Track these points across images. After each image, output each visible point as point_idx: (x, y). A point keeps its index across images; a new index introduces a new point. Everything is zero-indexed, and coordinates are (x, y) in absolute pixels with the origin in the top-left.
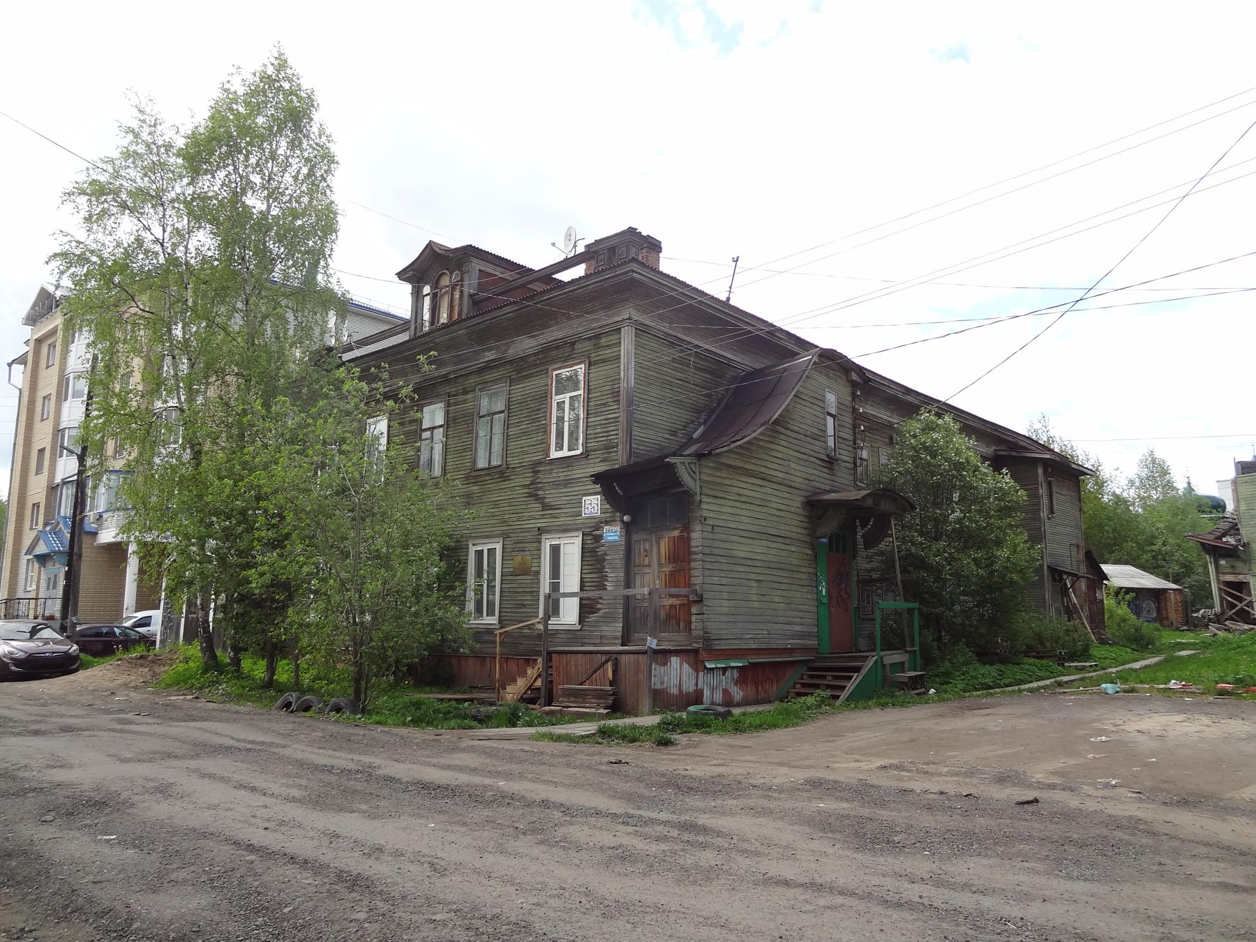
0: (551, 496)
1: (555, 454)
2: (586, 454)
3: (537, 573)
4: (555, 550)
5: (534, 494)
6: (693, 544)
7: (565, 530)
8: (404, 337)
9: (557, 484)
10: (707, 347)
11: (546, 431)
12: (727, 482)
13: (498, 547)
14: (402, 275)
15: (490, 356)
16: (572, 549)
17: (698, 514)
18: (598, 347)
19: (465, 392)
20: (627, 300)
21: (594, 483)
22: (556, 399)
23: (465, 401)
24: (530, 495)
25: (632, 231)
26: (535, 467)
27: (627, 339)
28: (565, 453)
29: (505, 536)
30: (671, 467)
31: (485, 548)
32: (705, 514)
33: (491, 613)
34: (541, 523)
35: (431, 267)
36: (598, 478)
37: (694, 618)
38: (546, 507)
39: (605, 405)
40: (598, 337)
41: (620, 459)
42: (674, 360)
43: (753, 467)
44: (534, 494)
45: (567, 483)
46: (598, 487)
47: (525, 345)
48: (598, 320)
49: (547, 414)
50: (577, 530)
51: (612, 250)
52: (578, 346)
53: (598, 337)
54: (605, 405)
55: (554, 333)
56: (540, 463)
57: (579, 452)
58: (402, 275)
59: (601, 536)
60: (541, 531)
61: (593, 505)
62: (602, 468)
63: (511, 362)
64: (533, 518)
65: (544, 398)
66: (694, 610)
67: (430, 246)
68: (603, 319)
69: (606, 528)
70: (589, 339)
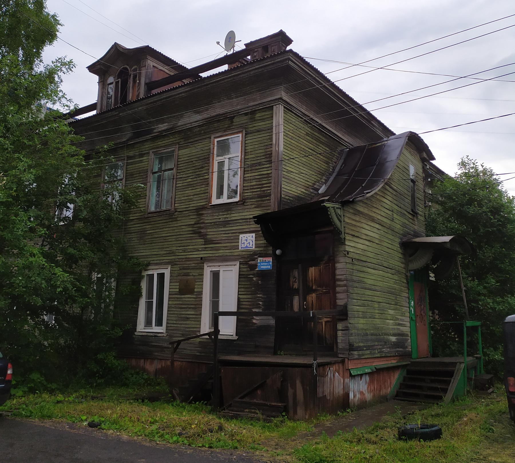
0: (212, 233)
1: (215, 201)
2: (243, 202)
3: (201, 293)
4: (216, 276)
5: (198, 232)
6: (338, 272)
7: (225, 259)
8: (94, 113)
9: (216, 225)
10: (320, 122)
11: (207, 183)
12: (358, 224)
13: (167, 272)
14: (92, 68)
15: (163, 127)
16: (230, 277)
17: (342, 249)
18: (253, 120)
19: (142, 155)
20: (281, 84)
21: (256, 223)
22: (217, 159)
23: (141, 162)
24: (194, 232)
25: (148, 46)
26: (199, 211)
27: (279, 114)
28: (224, 200)
29: (172, 263)
30: (326, 209)
31: (155, 273)
32: (348, 248)
33: (159, 323)
34: (203, 254)
35: (119, 65)
36: (259, 219)
37: (339, 333)
38: (208, 242)
39: (260, 164)
40: (253, 113)
41: (273, 206)
42: (307, 134)
43: (374, 215)
44: (198, 232)
45: (226, 223)
46: (258, 227)
47: (191, 119)
48: (254, 100)
49: (209, 172)
50: (235, 260)
51: (265, 48)
52: (236, 120)
53: (253, 113)
54: (260, 164)
55: (218, 109)
56: (203, 208)
57: (237, 199)
58: (92, 68)
59: (256, 266)
60: (203, 260)
61: (248, 241)
62: (258, 212)
63: (179, 132)
64: (196, 249)
65: (207, 159)
66: (340, 326)
67: (282, 39)
68: (257, 100)
69: (260, 259)
70: (246, 114)
